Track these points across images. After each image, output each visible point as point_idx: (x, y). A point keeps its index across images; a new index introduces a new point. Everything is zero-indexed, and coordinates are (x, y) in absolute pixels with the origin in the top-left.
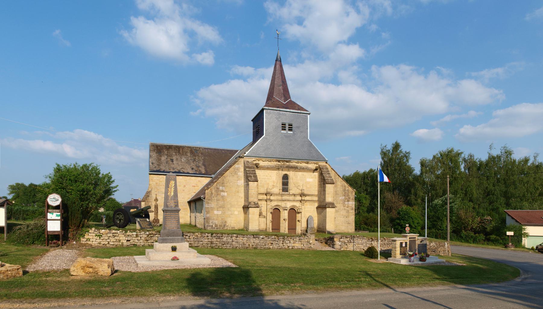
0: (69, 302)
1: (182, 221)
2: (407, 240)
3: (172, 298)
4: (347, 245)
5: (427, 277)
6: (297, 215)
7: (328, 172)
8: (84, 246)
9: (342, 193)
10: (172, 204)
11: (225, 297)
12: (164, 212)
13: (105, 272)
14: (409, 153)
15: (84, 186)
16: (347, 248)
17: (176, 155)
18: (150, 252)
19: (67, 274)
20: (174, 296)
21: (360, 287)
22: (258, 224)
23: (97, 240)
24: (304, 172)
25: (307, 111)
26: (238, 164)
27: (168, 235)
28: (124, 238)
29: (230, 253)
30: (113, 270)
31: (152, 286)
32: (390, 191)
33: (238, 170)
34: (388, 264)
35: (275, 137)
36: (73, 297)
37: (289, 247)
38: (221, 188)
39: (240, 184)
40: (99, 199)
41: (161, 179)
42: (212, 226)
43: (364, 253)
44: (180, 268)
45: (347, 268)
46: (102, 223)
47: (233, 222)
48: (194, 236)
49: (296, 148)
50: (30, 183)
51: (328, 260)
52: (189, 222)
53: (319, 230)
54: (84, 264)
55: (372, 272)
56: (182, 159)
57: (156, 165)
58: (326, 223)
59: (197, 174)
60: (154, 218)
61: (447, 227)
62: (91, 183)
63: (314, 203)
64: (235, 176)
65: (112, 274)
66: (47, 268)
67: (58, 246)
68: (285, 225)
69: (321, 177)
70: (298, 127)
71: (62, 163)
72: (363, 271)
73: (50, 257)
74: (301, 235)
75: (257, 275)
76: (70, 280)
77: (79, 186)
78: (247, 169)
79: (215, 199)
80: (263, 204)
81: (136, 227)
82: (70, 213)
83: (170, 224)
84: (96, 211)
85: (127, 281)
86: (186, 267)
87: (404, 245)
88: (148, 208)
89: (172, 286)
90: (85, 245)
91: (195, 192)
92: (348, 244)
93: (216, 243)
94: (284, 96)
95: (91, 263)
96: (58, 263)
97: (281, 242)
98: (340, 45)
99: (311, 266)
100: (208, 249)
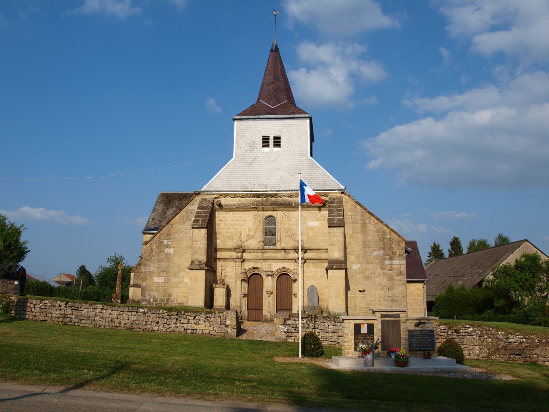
9: (379, 244)
25: (307, 113)
38: (165, 242)
42: (149, 300)
47: (180, 295)
63: (322, 264)
79: (156, 259)
87: (364, 330)
97: (174, 321)
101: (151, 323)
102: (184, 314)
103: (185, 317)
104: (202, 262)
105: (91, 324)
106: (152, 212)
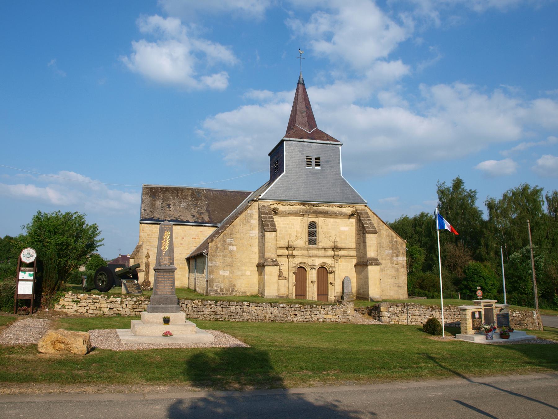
0: (33, 388)
1: (178, 284)
2: (482, 308)
3: (162, 388)
4: (398, 317)
5: (512, 361)
6: (329, 276)
7: (368, 217)
8: (58, 315)
10: (165, 261)
11: (231, 388)
12: (155, 272)
13: (80, 349)
14: (475, 192)
15: (63, 239)
16: (398, 321)
17: (174, 199)
18: (136, 324)
19: (34, 351)
20: (164, 385)
21: (420, 376)
22: (276, 288)
23: (73, 307)
24: (336, 218)
26: (251, 209)
27: (159, 302)
28: (106, 305)
29: (239, 328)
30: (89, 347)
31: (137, 370)
32: (452, 242)
33: (250, 216)
34: (457, 343)
35: (299, 175)
36: (38, 382)
37: (319, 319)
38: (228, 240)
39: (253, 235)
40: (80, 255)
41: (154, 229)
42: (217, 291)
43: (422, 328)
44: (173, 347)
45: (401, 350)
46: (82, 285)
48: (193, 304)
49: (326, 188)
50: (6, 236)
51: (373, 338)
52: (186, 286)
53: (360, 296)
54: (54, 338)
55: (436, 354)
56: (181, 205)
57: (149, 211)
58: (368, 287)
59: (200, 222)
60: (144, 280)
61: (533, 289)
62: (72, 235)
64: (247, 225)
65: (88, 352)
66: (12, 342)
67: (28, 314)
68: (314, 290)
69: (359, 225)
70: (327, 162)
71: (49, 211)
72: (422, 353)
73: (16, 328)
74: (335, 302)
75: (276, 359)
76: (36, 359)
77: (58, 238)
78: (262, 216)
80: (283, 261)
81: (121, 290)
82: (45, 272)
83: (162, 287)
84: (76, 270)
85: (105, 363)
86: (181, 346)
87: (477, 316)
88: (137, 266)
89: (162, 371)
90: (59, 313)
91: (195, 246)
92: (399, 315)
93: (222, 313)
94: (309, 124)
95: (63, 337)
96: (25, 336)
97: (309, 312)
98: (379, 62)
99: (350, 346)
100: (210, 322)
101: (291, 316)
102: (316, 307)
103: (317, 309)
104: (274, 260)
105: (240, 319)
106: (142, 203)
